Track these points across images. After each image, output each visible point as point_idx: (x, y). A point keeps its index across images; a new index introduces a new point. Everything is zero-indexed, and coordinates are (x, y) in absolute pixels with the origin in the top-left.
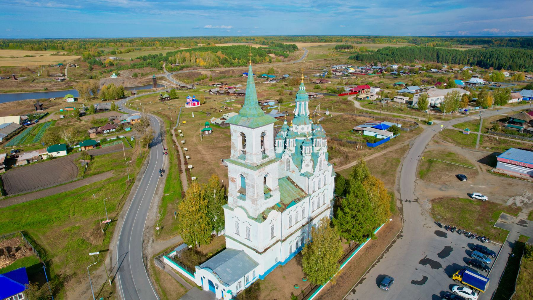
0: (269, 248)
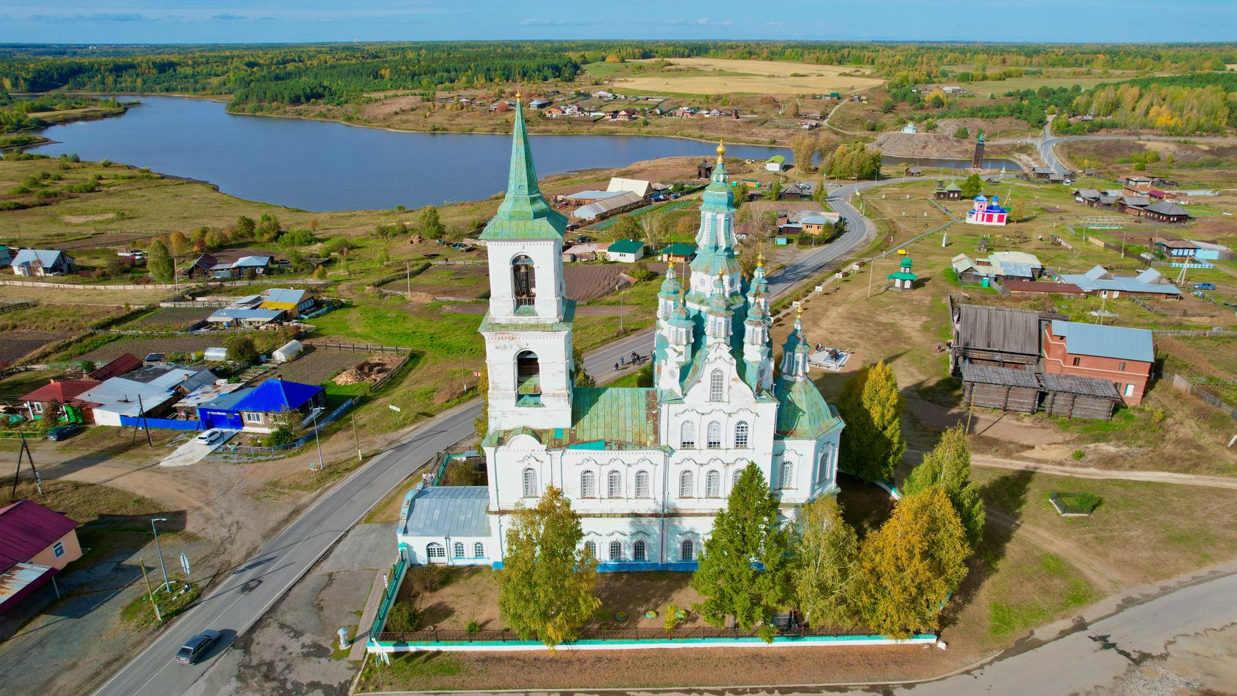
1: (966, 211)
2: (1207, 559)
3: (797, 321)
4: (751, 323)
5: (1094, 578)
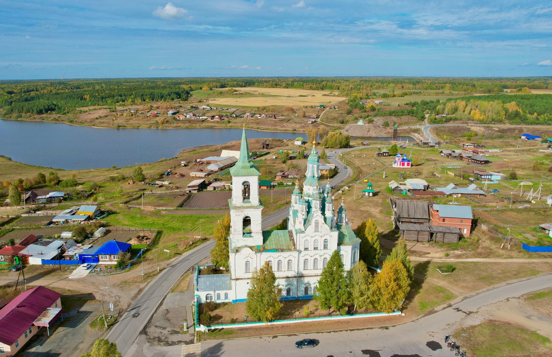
0: (242, 279)
1: (392, 161)
2: (492, 283)
3: (342, 202)
4: (328, 203)
5: (454, 292)
